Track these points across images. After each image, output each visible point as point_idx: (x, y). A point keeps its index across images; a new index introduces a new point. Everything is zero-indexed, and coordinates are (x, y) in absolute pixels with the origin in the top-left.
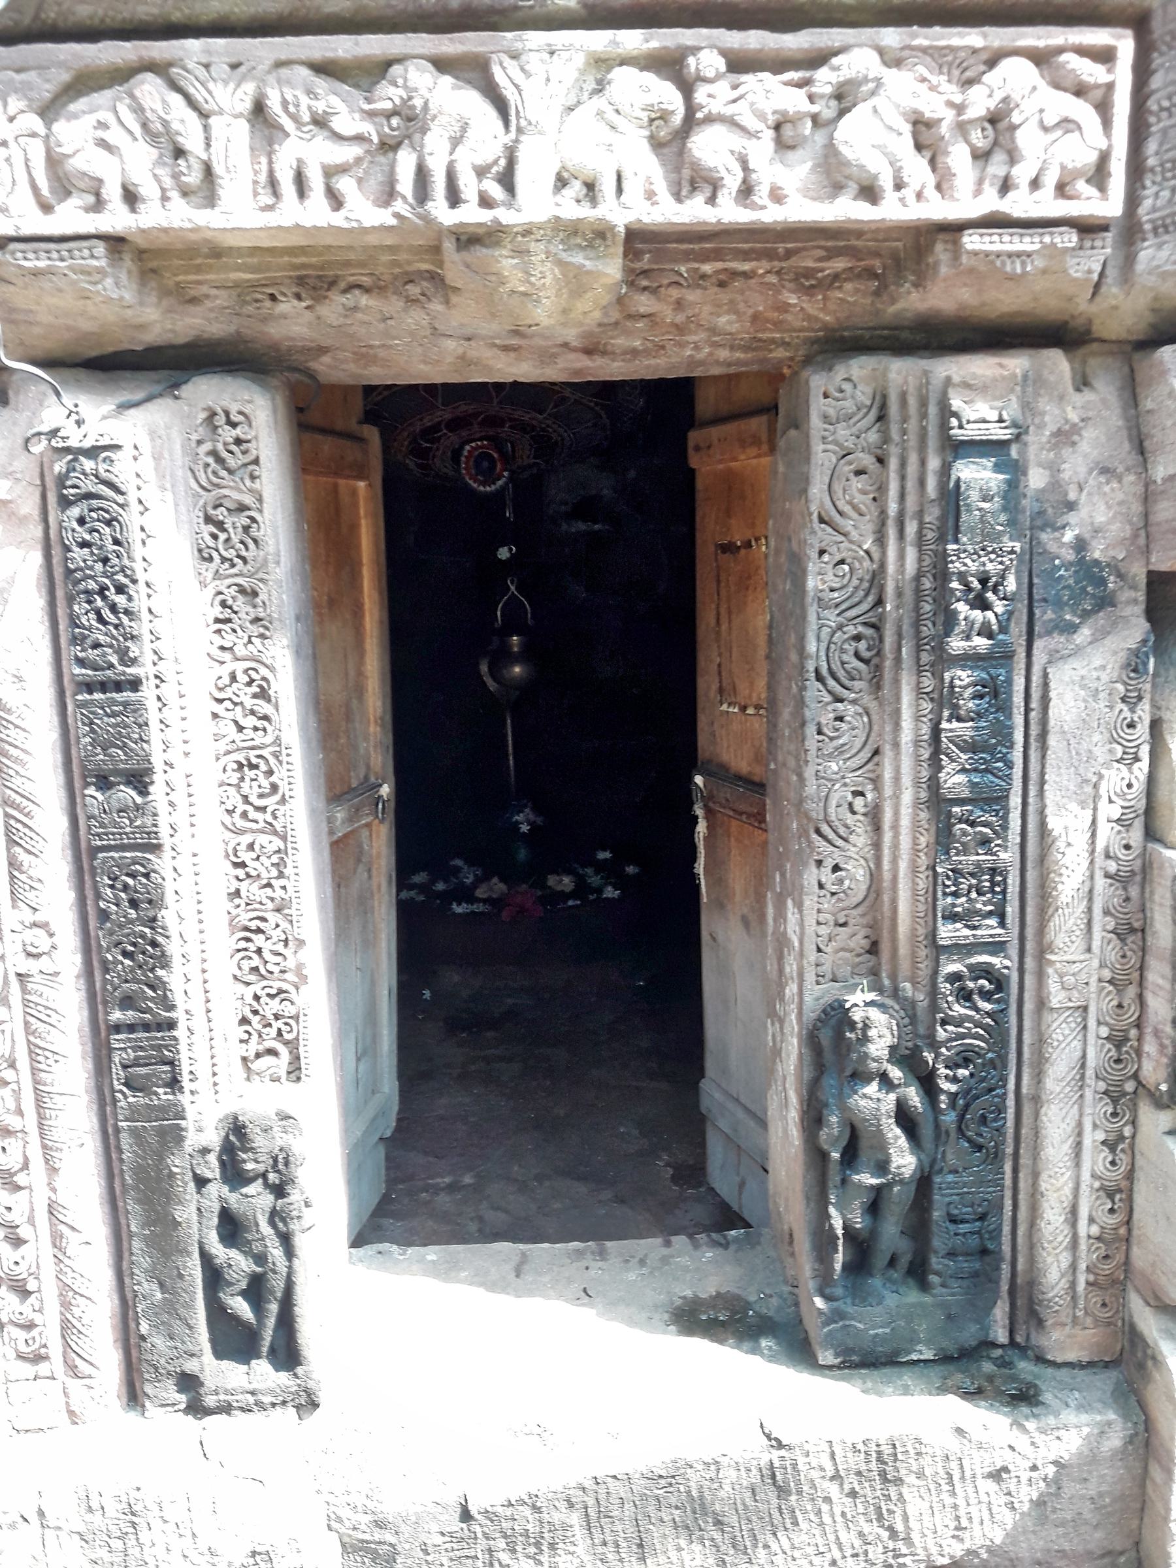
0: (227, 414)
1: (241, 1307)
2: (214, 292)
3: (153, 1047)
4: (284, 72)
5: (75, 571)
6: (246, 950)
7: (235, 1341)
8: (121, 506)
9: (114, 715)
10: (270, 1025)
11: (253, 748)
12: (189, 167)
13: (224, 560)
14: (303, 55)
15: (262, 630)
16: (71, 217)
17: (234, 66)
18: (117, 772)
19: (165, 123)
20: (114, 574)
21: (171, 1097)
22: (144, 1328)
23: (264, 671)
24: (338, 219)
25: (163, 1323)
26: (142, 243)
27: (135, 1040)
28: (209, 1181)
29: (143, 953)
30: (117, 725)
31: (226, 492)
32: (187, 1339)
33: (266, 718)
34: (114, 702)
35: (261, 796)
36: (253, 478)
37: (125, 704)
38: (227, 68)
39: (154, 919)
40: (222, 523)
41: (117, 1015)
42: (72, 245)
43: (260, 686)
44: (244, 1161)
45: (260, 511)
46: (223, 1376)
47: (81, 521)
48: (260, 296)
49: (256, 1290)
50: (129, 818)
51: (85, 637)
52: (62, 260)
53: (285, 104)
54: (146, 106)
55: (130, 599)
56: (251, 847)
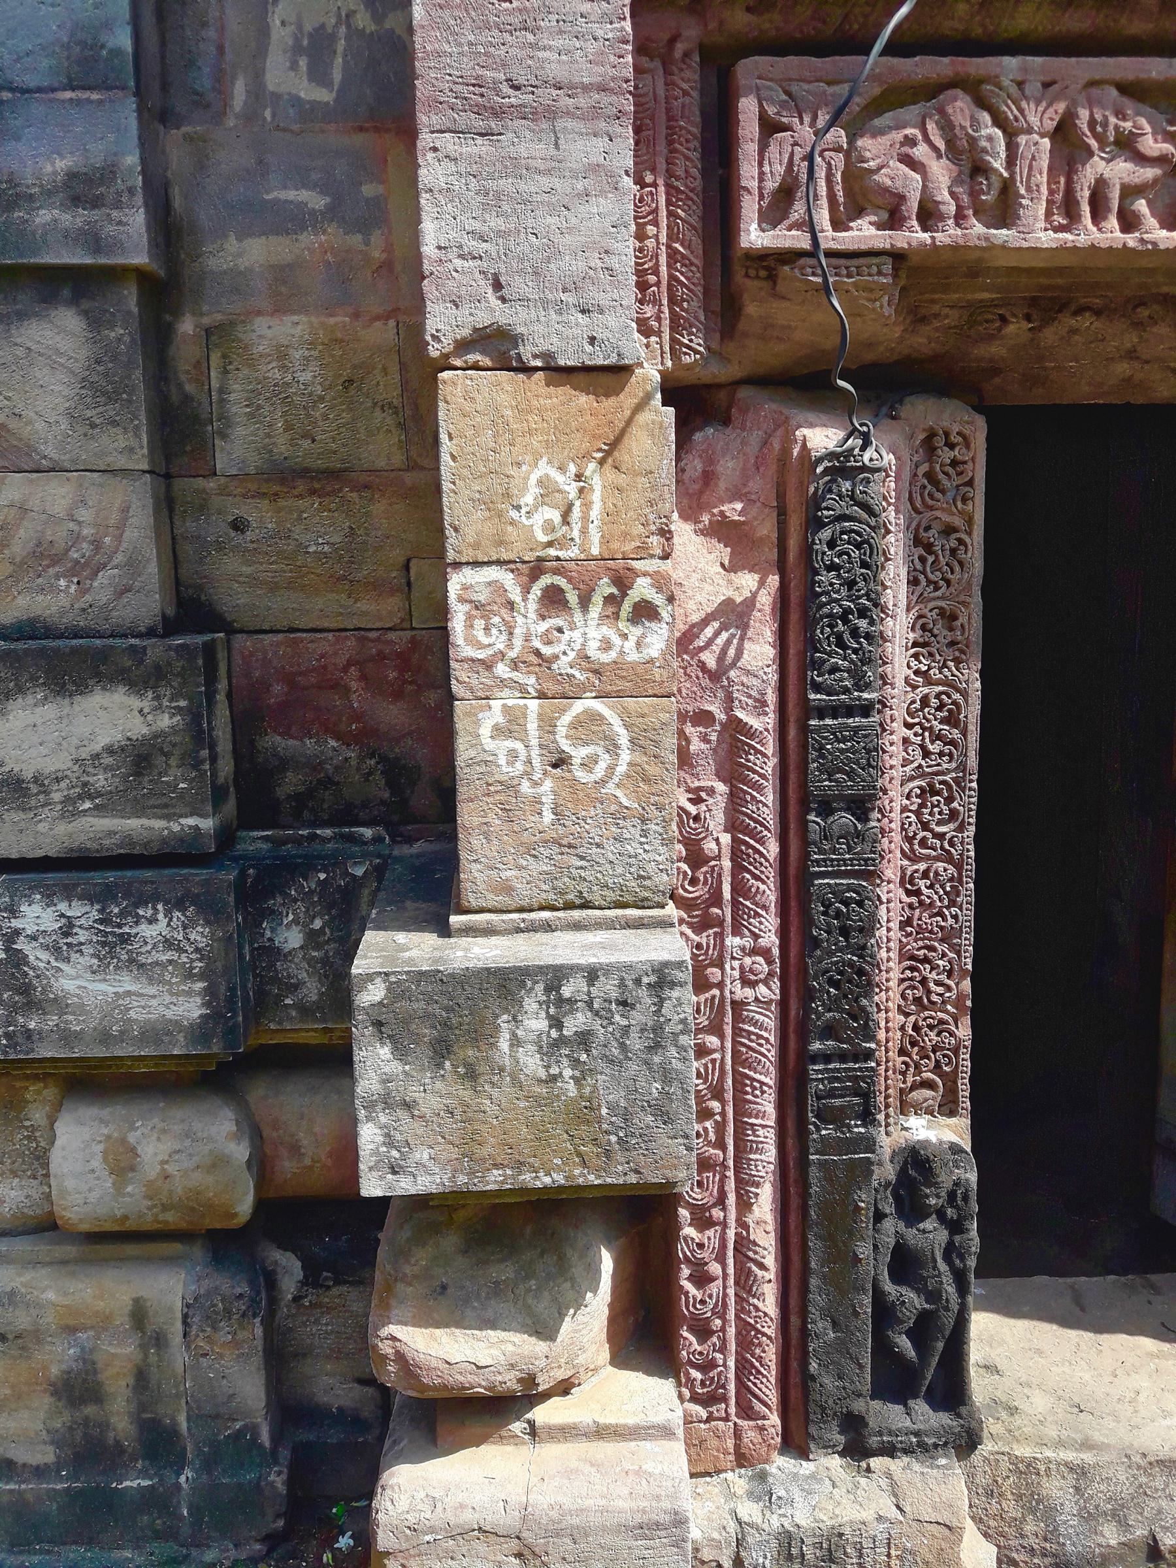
0: (947, 434)
1: (904, 1344)
2: (946, 311)
3: (849, 1079)
4: (1095, 92)
5: (821, 594)
6: (911, 979)
7: (896, 1382)
8: (873, 528)
9: (844, 740)
10: (928, 1058)
11: (937, 774)
12: (989, 186)
13: (929, 582)
14: (1118, 76)
15: (957, 654)
16: (864, 232)
17: (1046, 85)
18: (841, 797)
19: (973, 141)
20: (859, 597)
21: (862, 1130)
22: (814, 1366)
23: (956, 696)
24: (1131, 240)
25: (833, 1363)
26: (914, 260)
27: (833, 1070)
28: (886, 1216)
29: (850, 982)
30: (847, 750)
31: (938, 514)
32: (856, 1379)
33: (953, 743)
34: (847, 727)
35: (939, 823)
36: (964, 500)
37: (856, 730)
38: (1039, 85)
39: (864, 947)
40: (932, 545)
41: (816, 1046)
42: (862, 261)
43: (949, 711)
44: (927, 1196)
45: (970, 534)
46: (889, 1416)
47: (831, 544)
48: (990, 317)
49: (921, 1331)
50: (848, 844)
51: (824, 661)
52: (849, 276)
53: (1092, 123)
54: (957, 124)
55: (872, 623)
56: (925, 875)
